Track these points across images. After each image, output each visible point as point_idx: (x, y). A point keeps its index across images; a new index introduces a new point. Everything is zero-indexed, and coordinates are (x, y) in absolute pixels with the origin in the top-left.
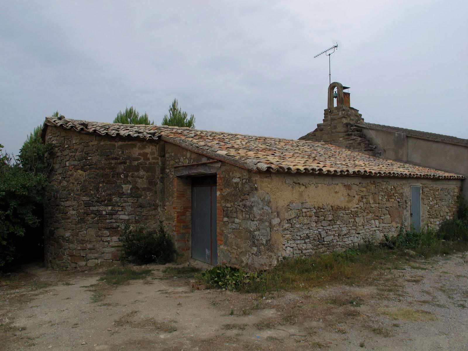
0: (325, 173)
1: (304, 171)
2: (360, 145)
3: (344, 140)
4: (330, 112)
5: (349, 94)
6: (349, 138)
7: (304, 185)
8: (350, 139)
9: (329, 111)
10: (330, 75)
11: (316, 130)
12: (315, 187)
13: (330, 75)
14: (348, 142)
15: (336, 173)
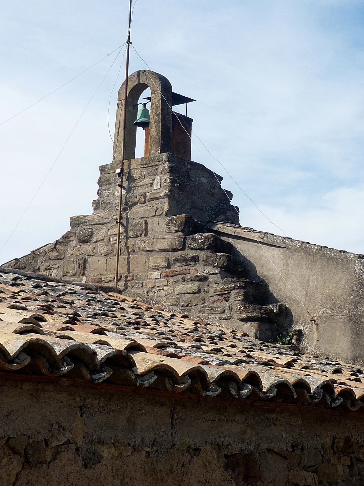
0: (146, 384)
1: (27, 360)
2: (227, 299)
3: (164, 281)
4: (119, 174)
5: (188, 122)
6: (188, 272)
7: (15, 452)
8: (189, 276)
9: (118, 171)
10: (129, 43)
11: (66, 238)
12: (80, 462)
13: (129, 43)
14: (179, 288)
15: (198, 386)
